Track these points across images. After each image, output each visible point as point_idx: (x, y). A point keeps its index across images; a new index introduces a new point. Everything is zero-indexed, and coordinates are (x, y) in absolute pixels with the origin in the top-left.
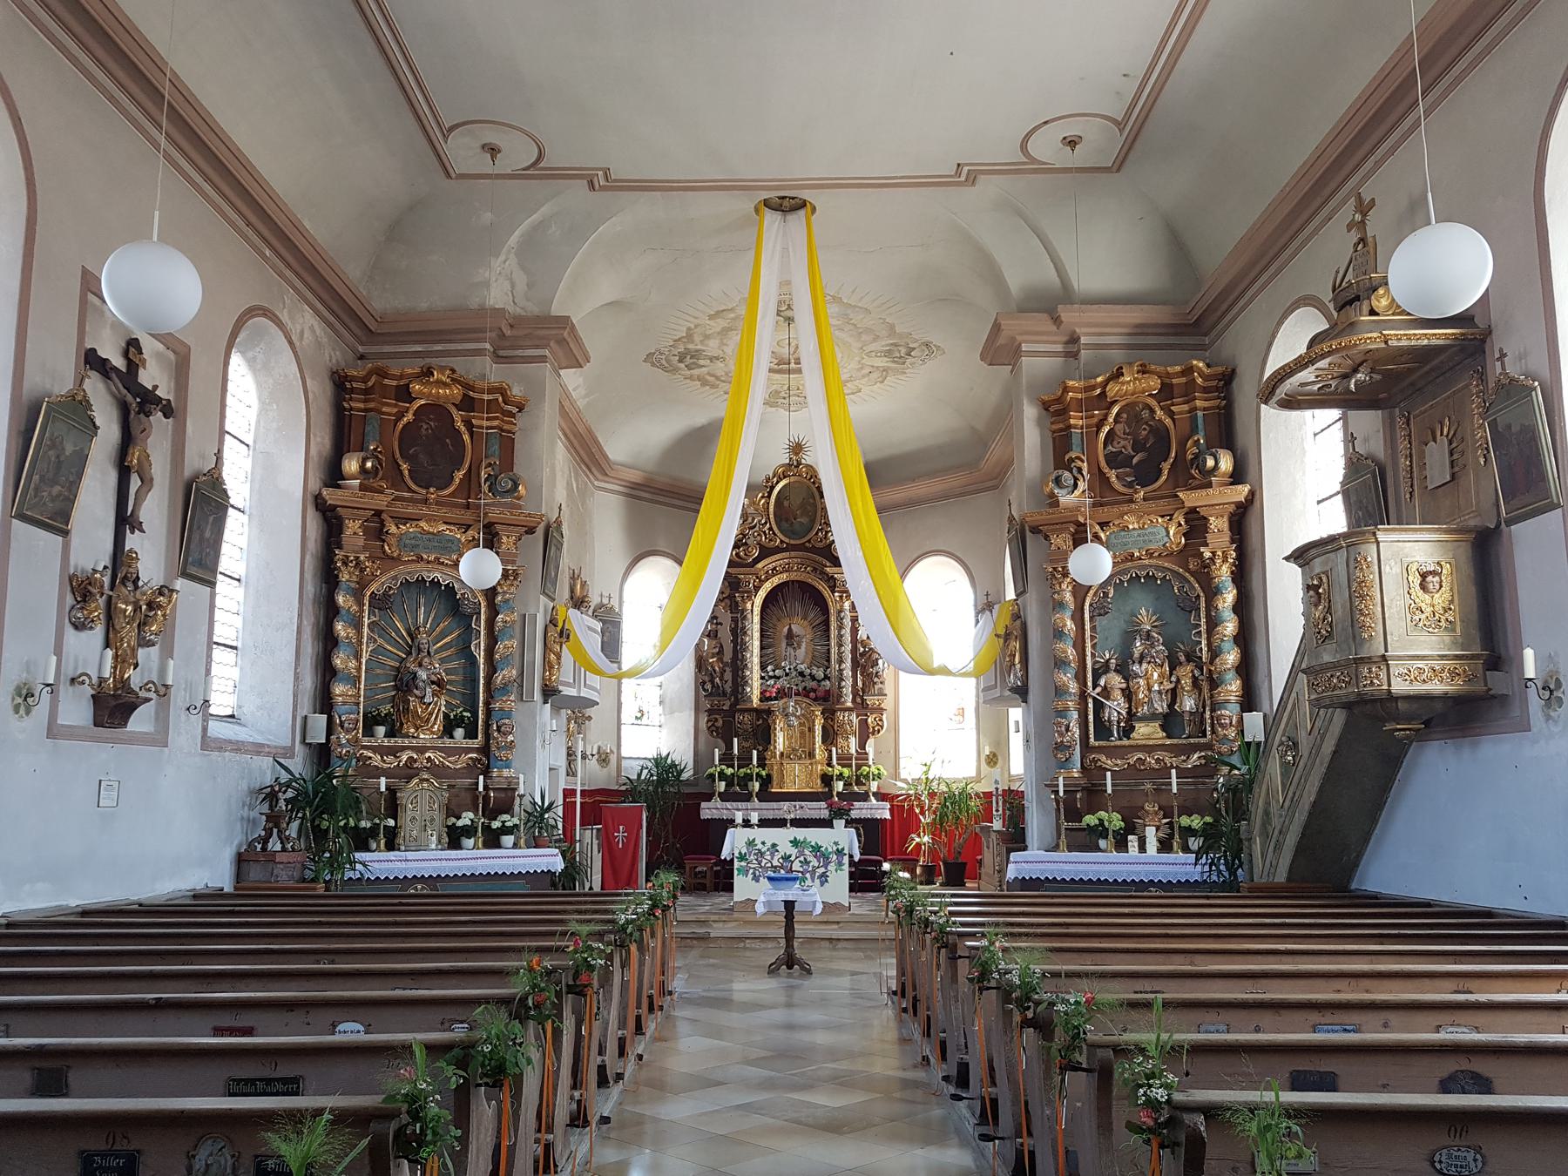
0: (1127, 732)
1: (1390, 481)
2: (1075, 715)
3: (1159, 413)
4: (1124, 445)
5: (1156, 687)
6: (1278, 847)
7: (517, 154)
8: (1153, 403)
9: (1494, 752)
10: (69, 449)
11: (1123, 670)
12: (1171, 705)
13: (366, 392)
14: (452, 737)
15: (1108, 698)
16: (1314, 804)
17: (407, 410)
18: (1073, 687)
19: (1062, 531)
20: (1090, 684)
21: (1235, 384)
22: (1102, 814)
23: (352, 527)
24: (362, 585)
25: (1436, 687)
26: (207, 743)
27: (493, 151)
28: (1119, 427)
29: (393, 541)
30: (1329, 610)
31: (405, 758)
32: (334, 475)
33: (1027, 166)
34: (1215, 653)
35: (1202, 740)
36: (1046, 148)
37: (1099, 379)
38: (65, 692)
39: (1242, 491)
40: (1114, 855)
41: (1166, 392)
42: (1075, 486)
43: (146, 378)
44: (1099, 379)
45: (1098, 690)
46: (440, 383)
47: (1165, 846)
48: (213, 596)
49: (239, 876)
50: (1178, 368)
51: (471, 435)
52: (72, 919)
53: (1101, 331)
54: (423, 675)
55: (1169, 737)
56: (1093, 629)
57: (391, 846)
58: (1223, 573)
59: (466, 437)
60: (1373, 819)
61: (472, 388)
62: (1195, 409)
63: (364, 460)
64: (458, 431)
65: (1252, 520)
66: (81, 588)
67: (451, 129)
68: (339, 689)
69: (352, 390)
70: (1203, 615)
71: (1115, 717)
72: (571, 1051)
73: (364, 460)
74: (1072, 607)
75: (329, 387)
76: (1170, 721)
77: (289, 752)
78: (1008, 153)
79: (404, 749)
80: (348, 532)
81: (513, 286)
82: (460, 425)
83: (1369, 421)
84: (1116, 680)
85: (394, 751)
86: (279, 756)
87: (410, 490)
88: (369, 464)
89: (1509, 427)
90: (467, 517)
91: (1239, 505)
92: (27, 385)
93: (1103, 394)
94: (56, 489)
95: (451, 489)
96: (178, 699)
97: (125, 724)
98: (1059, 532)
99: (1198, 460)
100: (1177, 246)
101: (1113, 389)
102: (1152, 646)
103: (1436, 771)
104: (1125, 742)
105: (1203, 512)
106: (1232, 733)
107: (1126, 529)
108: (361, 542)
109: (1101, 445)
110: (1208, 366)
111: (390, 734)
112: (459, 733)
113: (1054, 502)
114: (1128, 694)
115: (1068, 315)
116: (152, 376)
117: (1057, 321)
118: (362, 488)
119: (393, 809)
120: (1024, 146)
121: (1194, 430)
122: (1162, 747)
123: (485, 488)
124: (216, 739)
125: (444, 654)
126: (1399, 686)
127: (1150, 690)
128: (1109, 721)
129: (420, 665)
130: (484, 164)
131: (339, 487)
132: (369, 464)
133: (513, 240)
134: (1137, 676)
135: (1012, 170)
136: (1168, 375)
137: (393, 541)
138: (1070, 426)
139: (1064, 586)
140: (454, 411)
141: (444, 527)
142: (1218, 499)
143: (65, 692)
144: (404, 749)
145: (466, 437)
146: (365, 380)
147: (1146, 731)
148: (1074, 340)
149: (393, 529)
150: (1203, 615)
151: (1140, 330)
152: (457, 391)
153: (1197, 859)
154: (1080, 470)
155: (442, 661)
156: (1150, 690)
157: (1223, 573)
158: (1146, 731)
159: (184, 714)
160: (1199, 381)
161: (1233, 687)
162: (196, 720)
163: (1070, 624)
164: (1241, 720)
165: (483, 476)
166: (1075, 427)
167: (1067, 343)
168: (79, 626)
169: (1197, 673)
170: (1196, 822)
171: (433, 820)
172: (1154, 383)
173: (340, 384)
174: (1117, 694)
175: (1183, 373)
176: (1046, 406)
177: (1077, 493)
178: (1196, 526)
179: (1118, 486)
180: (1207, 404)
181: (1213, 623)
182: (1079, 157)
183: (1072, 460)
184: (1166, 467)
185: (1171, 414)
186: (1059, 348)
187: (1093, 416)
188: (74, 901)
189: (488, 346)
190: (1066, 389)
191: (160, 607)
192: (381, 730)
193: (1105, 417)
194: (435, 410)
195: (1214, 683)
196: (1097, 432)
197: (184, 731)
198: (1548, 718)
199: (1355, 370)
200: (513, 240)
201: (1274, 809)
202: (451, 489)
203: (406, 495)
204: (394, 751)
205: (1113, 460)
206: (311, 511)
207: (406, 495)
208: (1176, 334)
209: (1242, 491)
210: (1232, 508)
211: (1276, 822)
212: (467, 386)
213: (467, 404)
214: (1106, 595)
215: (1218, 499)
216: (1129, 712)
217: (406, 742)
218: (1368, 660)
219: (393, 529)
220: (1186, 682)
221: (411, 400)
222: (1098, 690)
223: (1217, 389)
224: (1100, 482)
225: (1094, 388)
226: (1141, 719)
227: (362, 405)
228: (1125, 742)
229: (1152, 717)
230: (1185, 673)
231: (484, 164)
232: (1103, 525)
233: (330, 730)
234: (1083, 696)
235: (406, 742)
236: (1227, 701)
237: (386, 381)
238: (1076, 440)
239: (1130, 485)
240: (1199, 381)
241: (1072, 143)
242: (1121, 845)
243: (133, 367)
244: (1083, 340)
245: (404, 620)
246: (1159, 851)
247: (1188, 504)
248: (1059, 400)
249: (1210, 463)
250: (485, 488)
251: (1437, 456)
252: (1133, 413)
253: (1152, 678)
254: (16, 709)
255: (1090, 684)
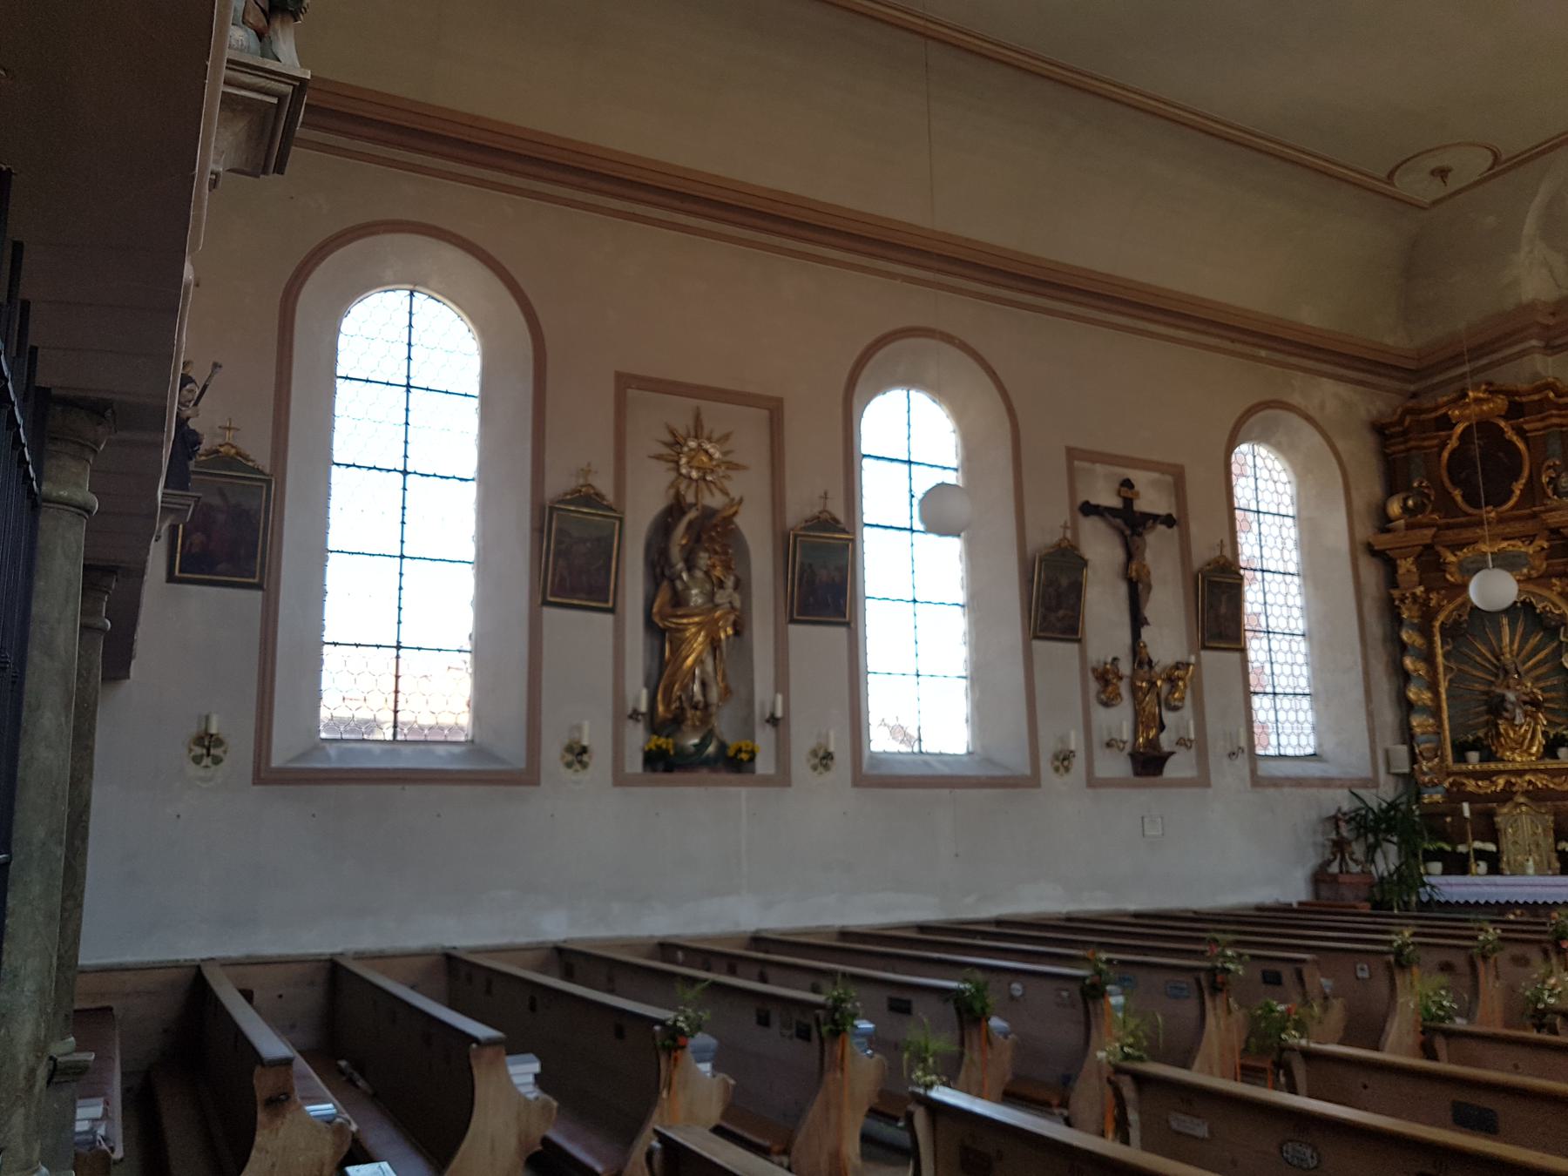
7: (1472, 164)
10: (1064, 582)
13: (1404, 433)
14: (1556, 757)
17: (1450, 437)
23: (1406, 565)
24: (1428, 615)
26: (1257, 781)
27: (1442, 173)
29: (1453, 569)
31: (1501, 782)
32: (1384, 522)
38: (1100, 754)
43: (1141, 505)
46: (1477, 401)
48: (1245, 661)
49: (1317, 893)
51: (1526, 440)
52: (1126, 920)
54: (1511, 696)
57: (1494, 869)
59: (1521, 446)
61: (1517, 393)
63: (1405, 500)
64: (1510, 442)
66: (1105, 677)
67: (1391, 175)
68: (1415, 721)
69: (1392, 436)
72: (879, 944)
73: (1405, 500)
75: (1370, 440)
77: (1372, 783)
79: (1499, 773)
80: (1401, 571)
81: (1551, 271)
82: (1510, 435)
85: (1488, 776)
86: (1352, 786)
87: (1467, 514)
88: (1410, 503)
90: (1530, 526)
92: (1029, 549)
94: (1061, 613)
95: (1511, 503)
96: (1217, 748)
97: (1161, 772)
108: (1416, 578)
111: (1488, 756)
112: (1474, 756)
116: (1151, 500)
118: (1409, 527)
119: (1493, 834)
123: (1550, 492)
124: (1263, 778)
125: (1534, 674)
129: (1508, 687)
130: (1435, 189)
131: (1388, 531)
132: (1410, 503)
133: (1530, 226)
137: (1453, 569)
140: (1502, 424)
141: (1504, 544)
143: (1100, 754)
144: (1499, 773)
145: (1521, 446)
146: (1401, 422)
149: (1452, 558)
152: (1501, 402)
155: (1537, 679)
159: (1226, 761)
162: (1242, 762)
165: (1545, 479)
168: (1106, 704)
171: (1538, 845)
173: (1380, 430)
188: (1132, 907)
189: (1534, 342)
191: (1179, 678)
192: (1474, 756)
194: (1485, 427)
197: (1228, 776)
200: (1530, 226)
202: (1511, 503)
203: (1463, 519)
204: (1488, 776)
206: (1366, 563)
207: (1463, 519)
212: (1509, 393)
213: (1515, 410)
217: (1501, 766)
219: (1452, 558)
221: (1453, 426)
227: (1402, 447)
231: (1435, 189)
233: (1414, 759)
235: (1501, 766)
237: (1423, 417)
243: (1128, 502)
245: (1487, 643)
250: (1550, 492)
254: (1057, 769)
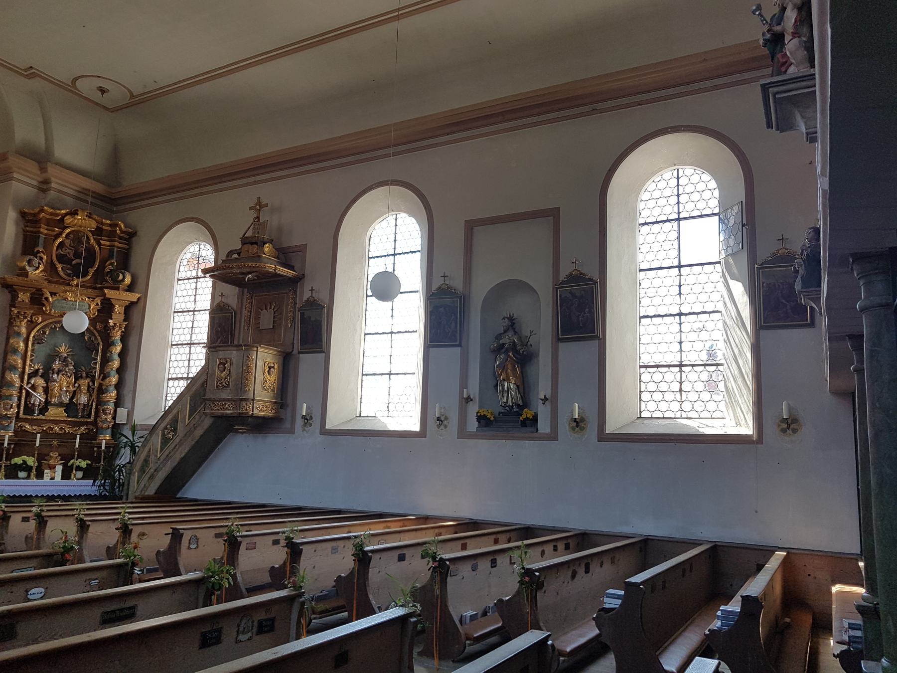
0: (44, 410)
1: (238, 319)
2: (16, 399)
3: (93, 242)
4: (68, 252)
5: (65, 389)
6: (152, 477)
8: (90, 234)
9: (274, 441)
11: (46, 377)
12: (71, 399)
15: (34, 391)
16: (182, 459)
18: (17, 382)
19: (26, 291)
20: (25, 382)
21: (134, 239)
22: (24, 457)
25: (266, 414)
28: (68, 242)
30: (229, 375)
33: (71, 87)
34: (105, 376)
35: (89, 420)
36: (85, 86)
37: (63, 212)
39: (134, 297)
40: (35, 481)
41: (98, 232)
42: (38, 268)
44: (63, 212)
45: (30, 385)
47: (66, 475)
50: (109, 222)
53: (63, 184)
55: (68, 416)
56: (33, 350)
58: (117, 335)
60: (200, 464)
62: (114, 246)
65: (135, 314)
70: (100, 354)
71: (37, 403)
74: (25, 336)
76: (70, 408)
78: (64, 76)
83: (231, 293)
84: (40, 382)
89: (310, 318)
91: (132, 303)
93: (62, 220)
98: (25, 292)
99: (113, 275)
100: (115, 157)
101: (68, 220)
102: (67, 365)
103: (239, 448)
104: (41, 417)
105: (113, 302)
106: (109, 417)
107: (66, 299)
109: (55, 248)
110: (125, 227)
113: (23, 273)
114: (46, 390)
115: (52, 170)
117: (43, 170)
120: (75, 80)
121: (111, 256)
122: (65, 422)
126: (256, 413)
127: (61, 390)
128: (34, 404)
134: (55, 381)
135: (59, 85)
136: (102, 223)
138: (39, 232)
139: (23, 323)
142: (120, 298)
147: (56, 413)
148: (46, 182)
150: (100, 354)
151: (85, 191)
153: (94, 482)
154: (41, 259)
156: (61, 390)
157: (117, 335)
158: (56, 413)
160: (118, 232)
161: (113, 394)
163: (22, 344)
164: (115, 411)
166: (42, 233)
167: (42, 182)
169: (91, 384)
170: (83, 464)
172: (94, 225)
174: (41, 390)
175: (110, 225)
176: (23, 214)
177: (38, 271)
178: (107, 308)
179: (61, 273)
180: (120, 245)
181: (106, 360)
182: (105, 100)
183: (38, 252)
184: (91, 271)
185: (99, 244)
186: (34, 183)
187: (54, 231)
190: (42, 211)
193: (61, 234)
195: (102, 390)
196: (54, 240)
198: (304, 430)
199: (250, 273)
201: (152, 459)
205: (61, 258)
208: (102, 200)
209: (134, 297)
210: (127, 303)
211: (152, 466)
214: (44, 333)
215: (120, 298)
216: (46, 399)
218: (246, 400)
220: (84, 388)
222: (30, 385)
223: (125, 239)
224: (51, 268)
225: (58, 215)
226: (55, 405)
228: (41, 417)
229: (61, 404)
230: (84, 383)
232: (52, 294)
234: (21, 388)
236: (109, 401)
238: (41, 241)
239: (69, 275)
240: (118, 232)
241: (103, 91)
242: (40, 475)
244: (53, 185)
246: (62, 479)
247: (108, 296)
248: (34, 215)
249: (121, 277)
251: (266, 318)
252: (76, 237)
253: (62, 384)
255: (25, 382)
